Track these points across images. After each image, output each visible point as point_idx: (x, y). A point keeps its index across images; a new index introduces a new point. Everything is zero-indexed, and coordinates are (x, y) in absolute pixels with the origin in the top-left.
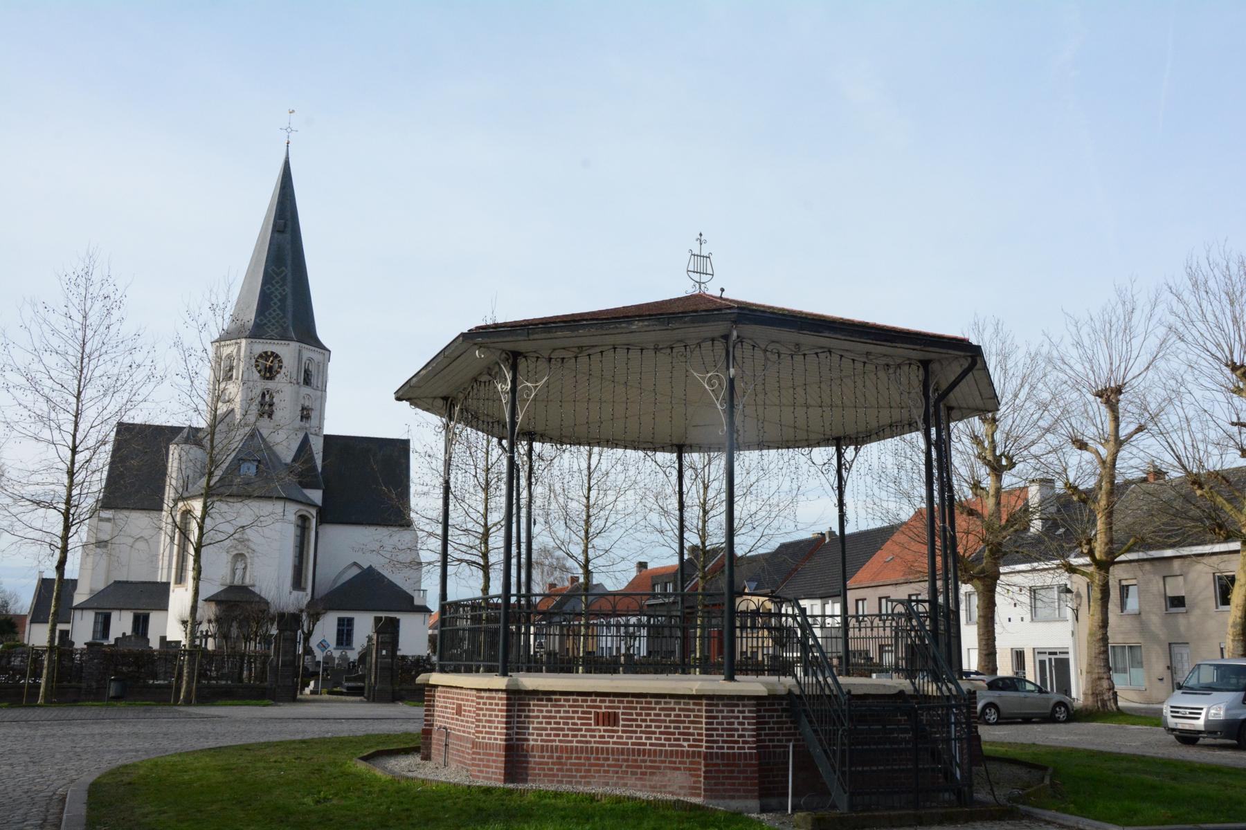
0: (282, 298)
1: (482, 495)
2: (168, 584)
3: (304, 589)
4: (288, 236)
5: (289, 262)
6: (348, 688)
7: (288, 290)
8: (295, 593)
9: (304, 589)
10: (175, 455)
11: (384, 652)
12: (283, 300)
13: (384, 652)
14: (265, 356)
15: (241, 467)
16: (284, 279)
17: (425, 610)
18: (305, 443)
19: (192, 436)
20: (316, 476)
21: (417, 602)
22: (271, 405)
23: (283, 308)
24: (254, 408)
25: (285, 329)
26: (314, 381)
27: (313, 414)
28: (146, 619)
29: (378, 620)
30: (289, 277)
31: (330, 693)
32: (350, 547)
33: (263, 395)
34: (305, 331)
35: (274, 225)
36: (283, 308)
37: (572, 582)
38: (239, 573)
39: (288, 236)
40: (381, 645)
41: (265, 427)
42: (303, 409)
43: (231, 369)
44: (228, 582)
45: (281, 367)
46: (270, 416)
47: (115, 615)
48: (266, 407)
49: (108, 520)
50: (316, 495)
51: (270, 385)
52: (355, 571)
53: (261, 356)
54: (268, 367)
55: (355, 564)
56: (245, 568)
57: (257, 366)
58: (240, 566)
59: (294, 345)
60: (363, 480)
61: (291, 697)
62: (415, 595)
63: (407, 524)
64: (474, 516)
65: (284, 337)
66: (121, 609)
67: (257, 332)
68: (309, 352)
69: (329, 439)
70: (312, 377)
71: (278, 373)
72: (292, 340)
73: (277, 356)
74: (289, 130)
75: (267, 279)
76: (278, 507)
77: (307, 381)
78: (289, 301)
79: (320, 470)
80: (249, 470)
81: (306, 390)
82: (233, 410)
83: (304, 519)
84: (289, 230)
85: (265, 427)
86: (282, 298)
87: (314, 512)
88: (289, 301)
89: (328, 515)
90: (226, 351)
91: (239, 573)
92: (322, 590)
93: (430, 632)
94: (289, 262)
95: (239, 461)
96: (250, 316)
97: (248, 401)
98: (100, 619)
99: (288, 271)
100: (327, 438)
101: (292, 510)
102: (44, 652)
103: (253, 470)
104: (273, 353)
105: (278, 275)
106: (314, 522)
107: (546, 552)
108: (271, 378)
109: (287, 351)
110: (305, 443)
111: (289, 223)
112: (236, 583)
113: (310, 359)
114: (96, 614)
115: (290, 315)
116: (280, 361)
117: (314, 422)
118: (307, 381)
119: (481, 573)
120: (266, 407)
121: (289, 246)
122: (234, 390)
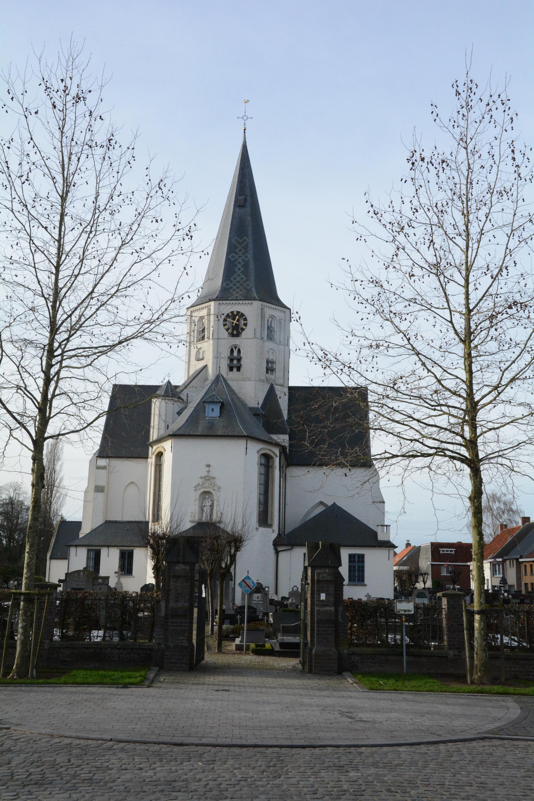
0: (246, 264)
1: (460, 349)
2: (147, 523)
3: (270, 526)
4: (248, 209)
5: (250, 232)
6: (283, 645)
7: (250, 256)
8: (262, 529)
9: (270, 526)
10: (157, 406)
11: (323, 596)
12: (246, 265)
13: (323, 596)
14: (232, 315)
15: (214, 413)
16: (246, 247)
17: (389, 545)
18: (271, 395)
19: (171, 392)
20: (283, 422)
21: (381, 537)
22: (239, 360)
23: (246, 273)
24: (224, 364)
25: (249, 291)
26: (276, 336)
27: (278, 367)
28: (130, 555)
29: (469, 546)
30: (251, 246)
31: (260, 651)
32: (316, 488)
33: (232, 351)
34: (265, 288)
35: (236, 201)
36: (246, 273)
37: (523, 522)
38: (207, 509)
39: (248, 209)
40: (318, 585)
41: (232, 377)
42: (268, 362)
43: (203, 330)
44: (197, 518)
45: (245, 325)
46: (239, 369)
47: (104, 552)
48: (235, 363)
49: (104, 468)
50: (284, 439)
51: (236, 341)
52: (321, 509)
53: (228, 316)
54: (235, 326)
55: (321, 503)
56: (212, 506)
57: (225, 325)
58: (208, 503)
59: (257, 304)
60: (327, 426)
61: (191, 663)
62: (379, 530)
63: (364, 461)
64: (450, 384)
65: (248, 297)
66: (108, 546)
67: (224, 295)
68: (270, 310)
69: (293, 391)
70: (275, 331)
71: (243, 330)
72: (255, 299)
73: (243, 315)
74: (245, 118)
75: (231, 249)
76: (241, 444)
77: (270, 337)
78: (251, 266)
79: (286, 417)
80: (213, 412)
81: (269, 345)
82: (206, 366)
83: (267, 459)
84: (248, 204)
85: (232, 377)
86: (246, 264)
87: (277, 451)
88: (251, 266)
89: (293, 458)
90: (197, 315)
91: (207, 509)
92: (289, 528)
93: (396, 568)
94: (250, 232)
95: (204, 402)
96: (218, 282)
97: (217, 357)
98: (92, 555)
99: (250, 240)
100: (291, 389)
101: (255, 449)
102: (8, 585)
103: (216, 413)
104: (238, 312)
105: (240, 244)
106: (277, 461)
107: (494, 498)
108: (238, 335)
109: (251, 309)
110: (271, 395)
111: (249, 198)
112: (204, 520)
113: (272, 317)
114: (88, 551)
115: (252, 278)
116: (245, 319)
117: (279, 373)
118: (270, 337)
119: (467, 470)
120: (235, 363)
121: (249, 218)
122: (208, 347)
